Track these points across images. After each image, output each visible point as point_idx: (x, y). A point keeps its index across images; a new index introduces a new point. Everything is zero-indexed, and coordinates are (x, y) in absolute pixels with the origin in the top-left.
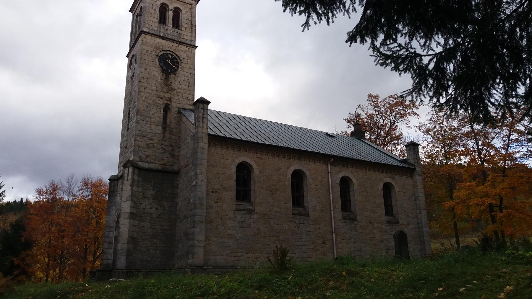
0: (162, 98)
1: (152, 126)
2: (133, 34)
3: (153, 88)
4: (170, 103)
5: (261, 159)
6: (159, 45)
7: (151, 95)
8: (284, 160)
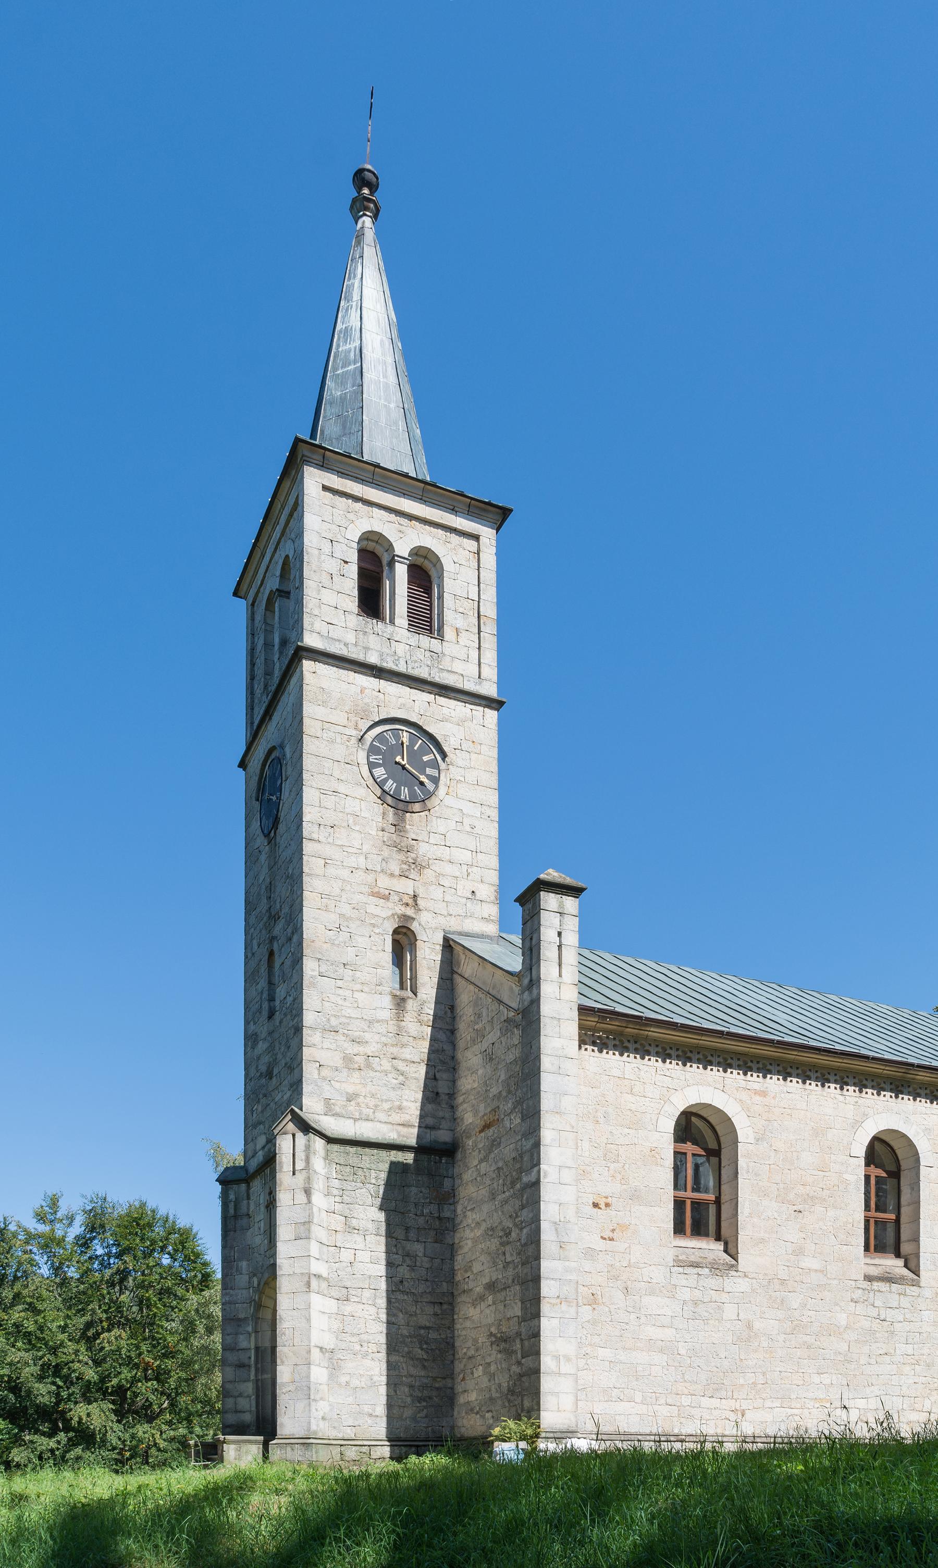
0: (386, 898)
1: (356, 995)
2: (257, 678)
3: (352, 861)
4: (414, 916)
5: (763, 1094)
6: (367, 700)
7: (348, 888)
8: (841, 1098)
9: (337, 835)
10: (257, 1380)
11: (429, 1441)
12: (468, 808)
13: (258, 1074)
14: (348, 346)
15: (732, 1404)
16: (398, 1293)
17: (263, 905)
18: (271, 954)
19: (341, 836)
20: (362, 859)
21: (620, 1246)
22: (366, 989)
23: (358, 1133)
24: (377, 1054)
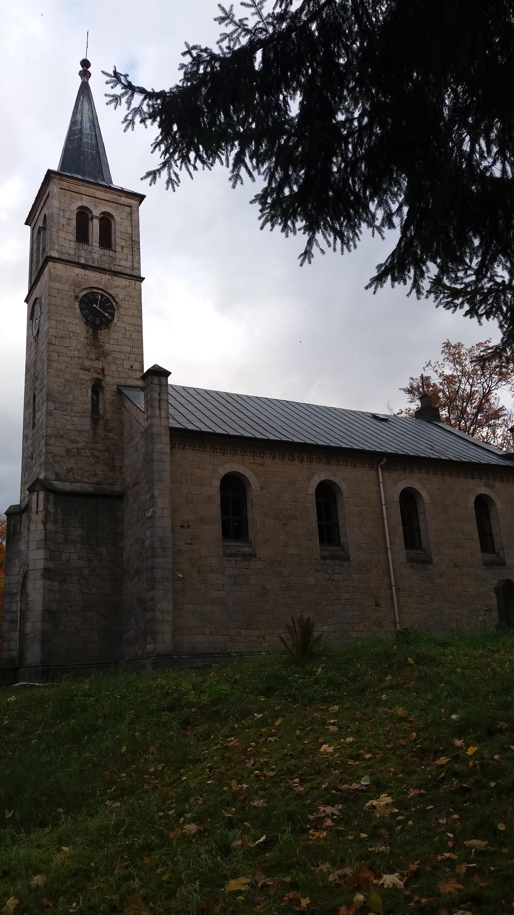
0: (89, 370)
1: (73, 418)
3: (72, 354)
4: (102, 378)
5: (263, 465)
7: (70, 366)
8: (301, 465)
9: (64, 341)
10: (20, 630)
11: (216, 654)
12: (128, 327)
14: (75, 128)
18: (35, 395)
20: (76, 353)
22: (78, 415)
23: (73, 489)
24: (83, 448)
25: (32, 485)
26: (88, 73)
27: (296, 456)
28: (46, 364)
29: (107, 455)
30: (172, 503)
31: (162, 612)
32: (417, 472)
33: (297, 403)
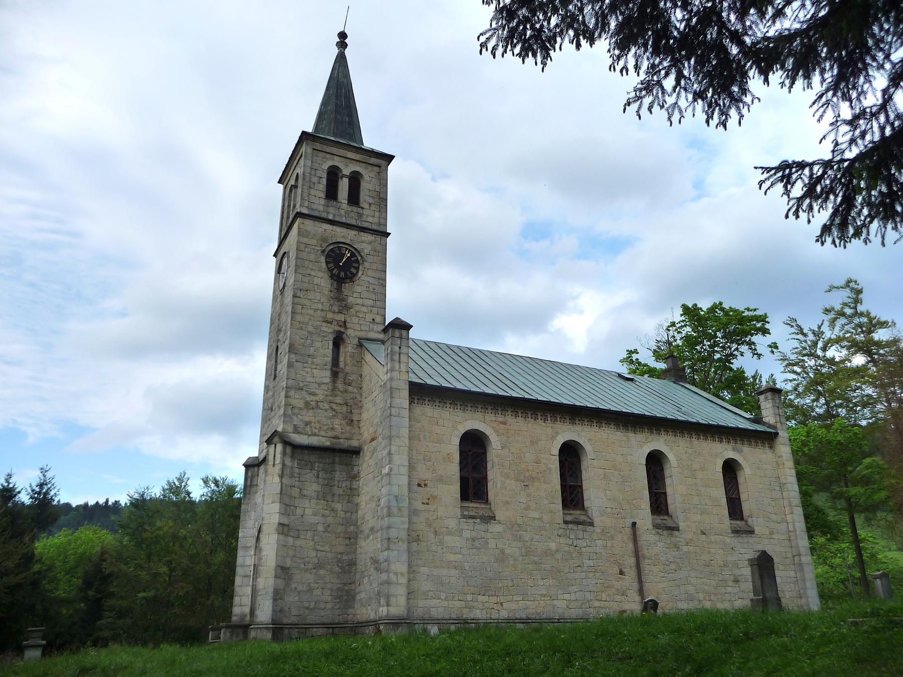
0: (331, 323)
1: (313, 370)
3: (315, 306)
5: (505, 423)
6: (326, 235)
8: (544, 424)
10: (253, 585)
13: (267, 408)
15: (494, 599)
16: (326, 533)
17: (276, 324)
18: (277, 347)
19: (311, 295)
21: (431, 507)
22: (318, 367)
25: (270, 437)
26: (345, 44)
27: (539, 415)
28: (290, 317)
29: (345, 409)
30: (409, 461)
31: (396, 574)
32: (664, 434)
33: (541, 360)
